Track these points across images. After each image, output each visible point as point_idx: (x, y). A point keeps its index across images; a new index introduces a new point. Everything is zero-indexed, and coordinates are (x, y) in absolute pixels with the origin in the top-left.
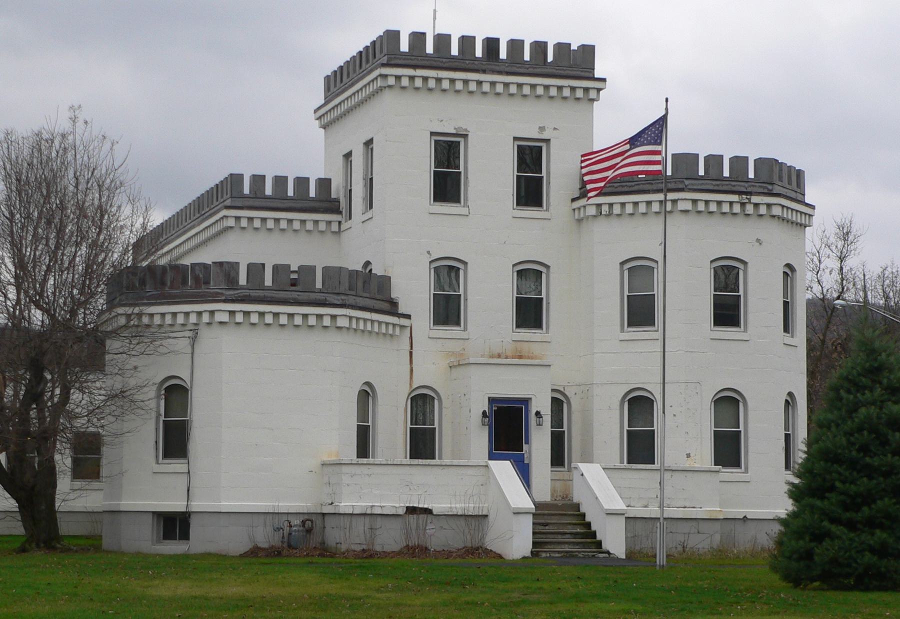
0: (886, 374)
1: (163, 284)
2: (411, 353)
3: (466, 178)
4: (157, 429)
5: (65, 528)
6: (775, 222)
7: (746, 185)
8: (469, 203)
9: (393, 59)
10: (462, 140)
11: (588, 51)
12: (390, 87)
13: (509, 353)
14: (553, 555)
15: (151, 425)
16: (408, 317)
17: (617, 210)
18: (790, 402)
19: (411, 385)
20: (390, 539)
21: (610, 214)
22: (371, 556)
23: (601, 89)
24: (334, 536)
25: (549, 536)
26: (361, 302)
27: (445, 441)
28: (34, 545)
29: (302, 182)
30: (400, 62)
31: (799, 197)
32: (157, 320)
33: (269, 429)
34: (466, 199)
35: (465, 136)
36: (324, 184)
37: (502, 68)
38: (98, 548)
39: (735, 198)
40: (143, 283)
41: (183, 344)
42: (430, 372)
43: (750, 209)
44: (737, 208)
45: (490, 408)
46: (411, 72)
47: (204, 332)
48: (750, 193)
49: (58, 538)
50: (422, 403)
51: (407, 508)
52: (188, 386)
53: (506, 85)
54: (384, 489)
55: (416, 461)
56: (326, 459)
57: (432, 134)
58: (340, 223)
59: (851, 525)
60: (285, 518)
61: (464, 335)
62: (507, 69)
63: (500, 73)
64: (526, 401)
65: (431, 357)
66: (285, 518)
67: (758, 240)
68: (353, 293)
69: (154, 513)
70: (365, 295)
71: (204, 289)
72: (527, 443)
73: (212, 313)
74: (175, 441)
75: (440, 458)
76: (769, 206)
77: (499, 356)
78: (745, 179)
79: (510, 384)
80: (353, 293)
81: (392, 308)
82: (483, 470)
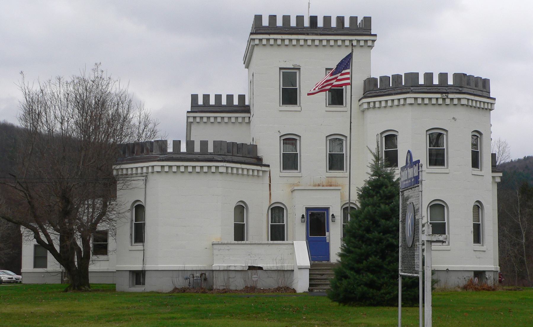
0: (384, 188)
1: (133, 153)
2: (270, 185)
3: (300, 91)
4: (131, 228)
5: (92, 280)
6: (461, 108)
7: (447, 88)
8: (301, 105)
9: (267, 30)
10: (297, 71)
11: (367, 20)
12: (257, 45)
13: (324, 184)
14: (321, 291)
15: (128, 225)
16: (268, 166)
17: (377, 105)
18: (478, 207)
19: (270, 202)
20: (238, 283)
21: (374, 107)
22: (226, 292)
23: (375, 41)
24: (219, 283)
25: (322, 281)
26: (235, 159)
27: (289, 231)
28: (72, 288)
29: (230, 98)
30: (263, 32)
31: (485, 94)
32: (130, 172)
33: (183, 228)
34: (300, 103)
35: (299, 69)
36: (242, 98)
37: (319, 32)
38: (114, 290)
39: (439, 96)
40: (124, 153)
41: (141, 184)
42: (280, 196)
43: (448, 101)
44: (440, 101)
45: (307, 213)
46: (267, 36)
47: (151, 177)
48: (448, 93)
49: (89, 285)
50: (277, 212)
51: (249, 266)
52: (143, 204)
53: (321, 41)
54: (235, 258)
55: (236, 242)
56: (215, 241)
57: (280, 69)
58: (249, 118)
59: (358, 271)
60: (190, 273)
61: (446, 171)
62: (322, 32)
63: (317, 34)
64: (327, 209)
65: (280, 187)
66: (190, 273)
67: (454, 118)
68: (231, 154)
69: (130, 271)
70: (238, 155)
71: (150, 155)
72: (328, 231)
73: (153, 167)
74: (139, 235)
75: (287, 240)
76: (459, 99)
77: (319, 186)
78: (446, 85)
79: (318, 201)
80: (231, 154)
81: (259, 161)
82: (291, 246)
